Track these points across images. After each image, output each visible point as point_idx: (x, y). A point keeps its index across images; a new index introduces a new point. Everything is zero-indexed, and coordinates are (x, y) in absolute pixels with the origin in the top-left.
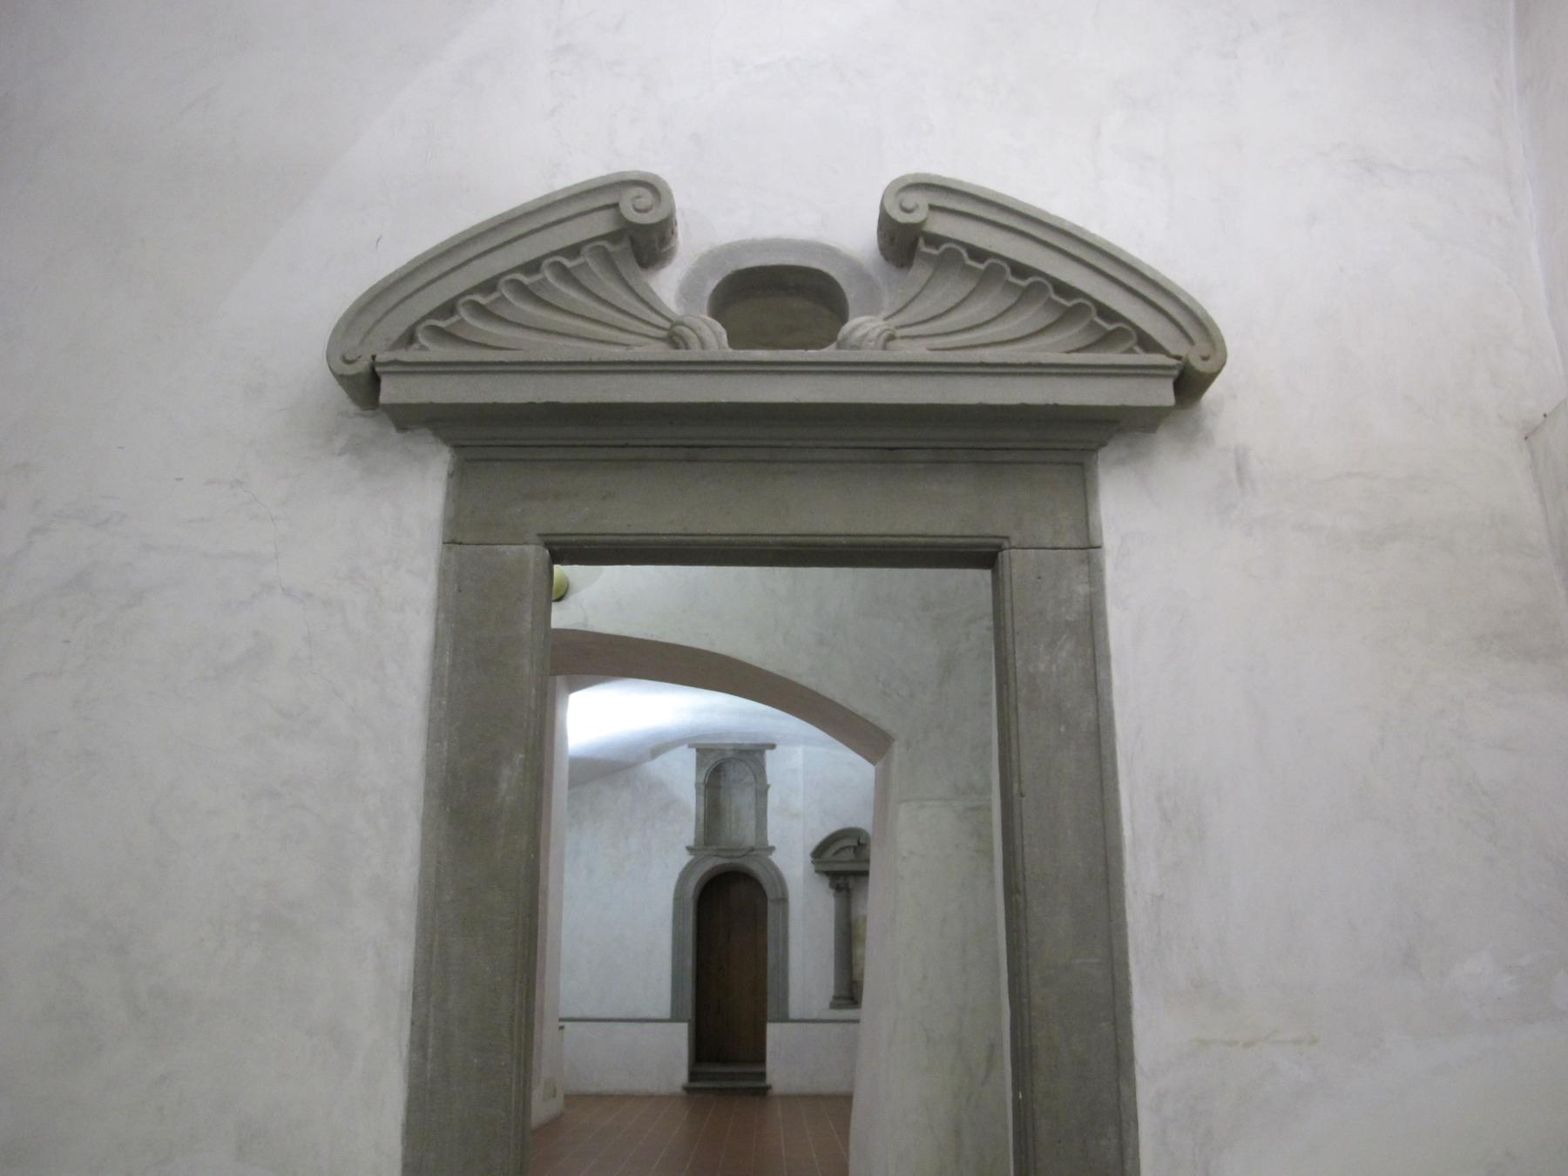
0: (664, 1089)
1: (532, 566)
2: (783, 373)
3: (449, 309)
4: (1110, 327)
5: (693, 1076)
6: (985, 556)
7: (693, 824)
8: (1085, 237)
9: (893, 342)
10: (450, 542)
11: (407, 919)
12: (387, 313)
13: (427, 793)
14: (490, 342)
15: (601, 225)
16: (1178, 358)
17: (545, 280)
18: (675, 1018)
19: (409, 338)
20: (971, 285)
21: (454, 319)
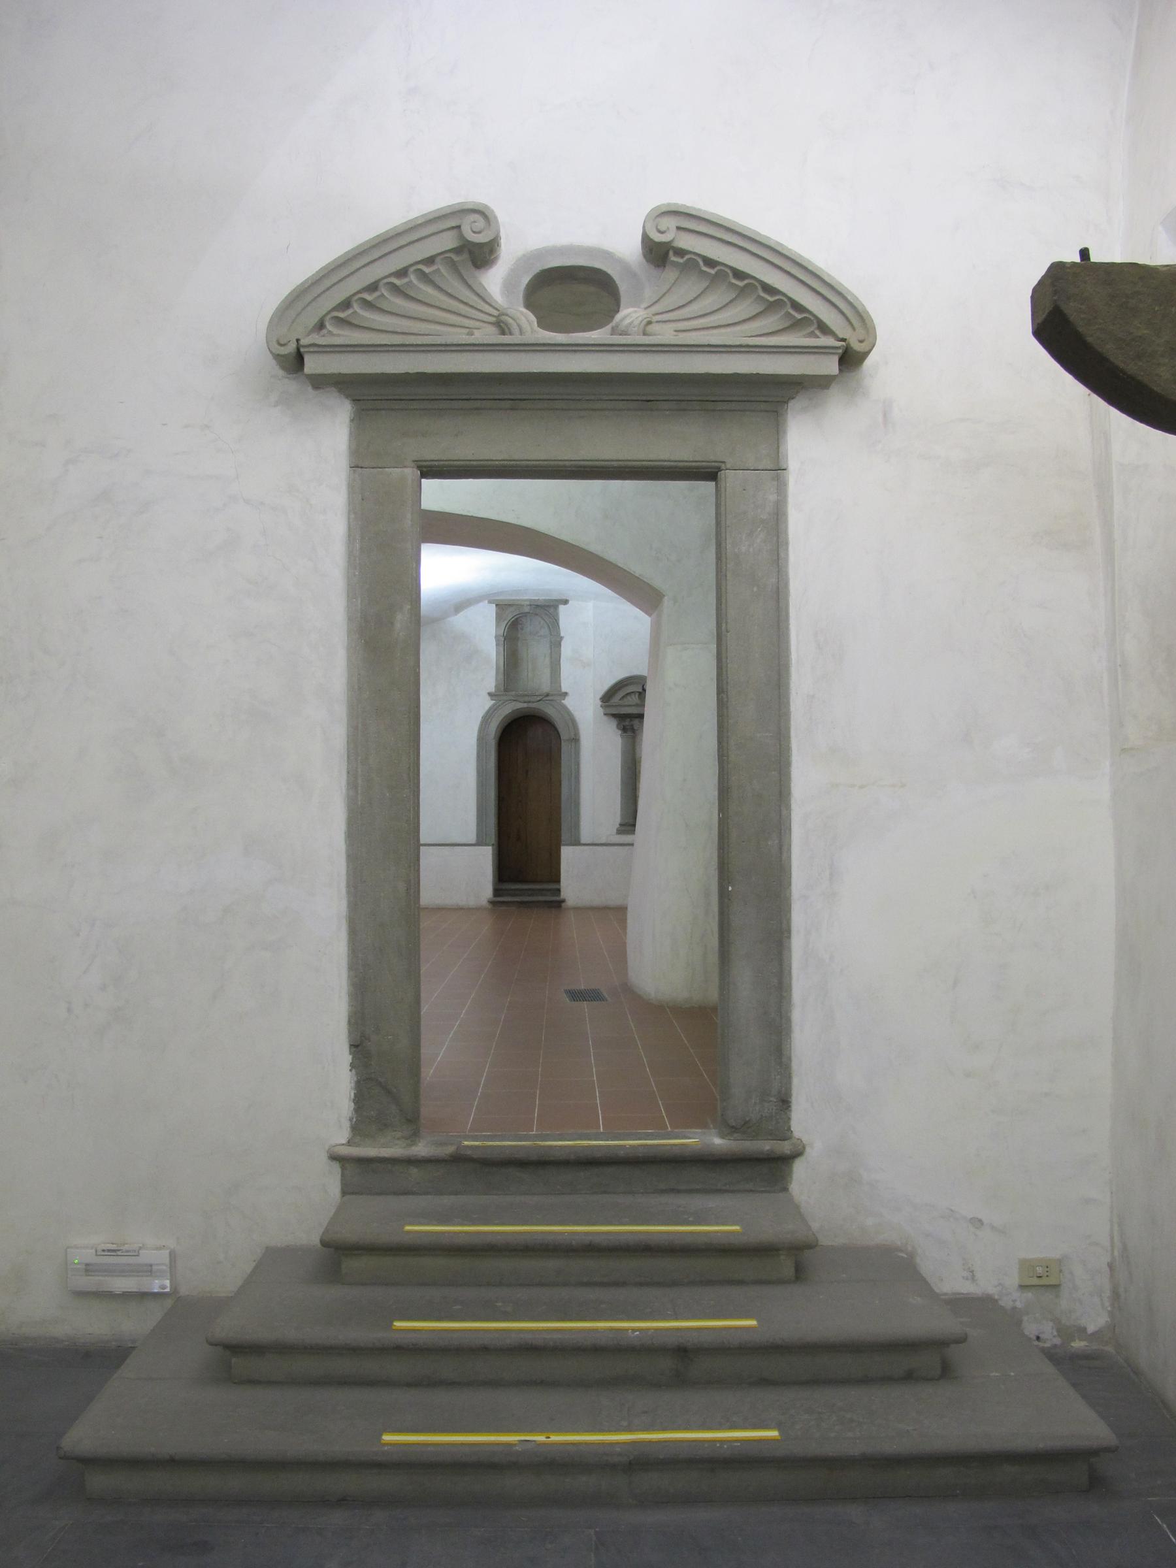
0: (472, 903)
1: (410, 482)
2: (575, 351)
3: (346, 304)
4: (799, 316)
5: (497, 892)
6: (710, 474)
7: (493, 672)
8: (784, 252)
9: (651, 327)
10: (355, 467)
11: (341, 710)
12: (304, 309)
13: (349, 632)
14: (373, 326)
15: (448, 242)
16: (844, 340)
17: (411, 282)
18: (480, 843)
19: (321, 326)
20: (705, 284)
21: (350, 311)
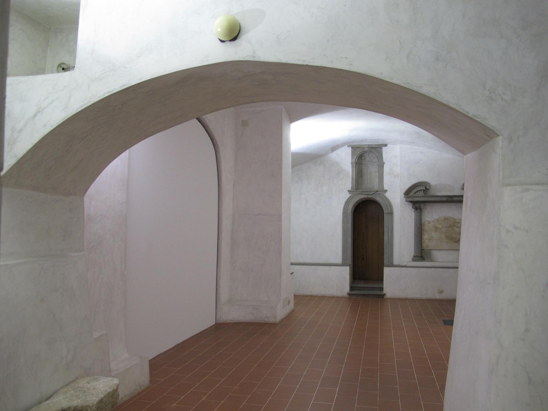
0: (339, 294)
5: (352, 288)
18: (343, 264)
